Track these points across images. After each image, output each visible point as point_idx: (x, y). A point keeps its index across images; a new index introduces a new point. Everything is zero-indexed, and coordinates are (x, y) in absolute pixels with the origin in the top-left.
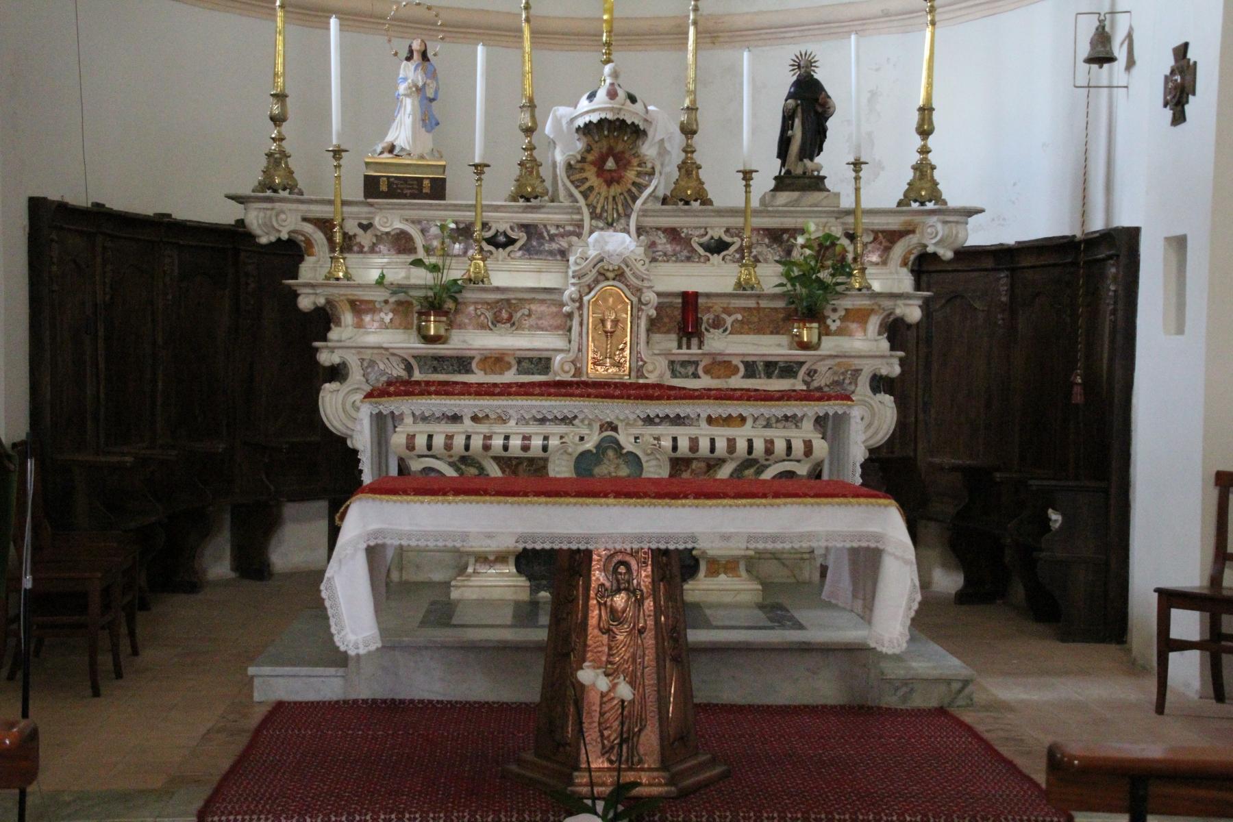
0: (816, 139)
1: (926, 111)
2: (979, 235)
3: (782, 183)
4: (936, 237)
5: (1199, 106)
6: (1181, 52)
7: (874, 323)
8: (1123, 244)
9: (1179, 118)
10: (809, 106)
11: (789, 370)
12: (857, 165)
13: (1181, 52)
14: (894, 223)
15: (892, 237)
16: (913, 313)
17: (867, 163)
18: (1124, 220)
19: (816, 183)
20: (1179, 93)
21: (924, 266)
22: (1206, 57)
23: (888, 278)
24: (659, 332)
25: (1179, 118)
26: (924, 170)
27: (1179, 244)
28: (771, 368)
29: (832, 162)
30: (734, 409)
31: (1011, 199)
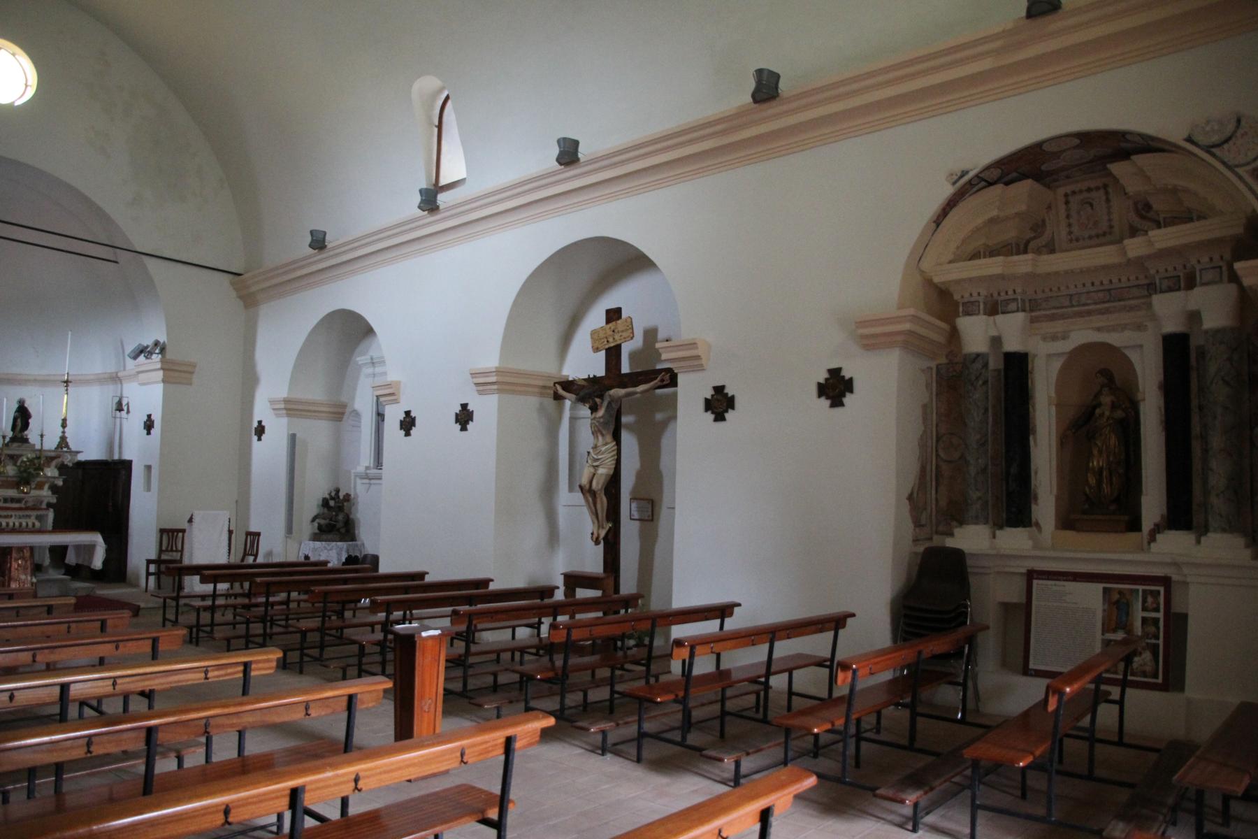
0: (26, 425)
1: (64, 421)
2: (81, 457)
3: (13, 440)
4: (68, 460)
5: (156, 430)
6: (149, 416)
7: (46, 486)
8: (127, 465)
9: (149, 433)
10: (23, 415)
11: (19, 501)
12: (42, 436)
13: (149, 416)
14: (53, 454)
15: (52, 458)
16: (60, 483)
17: (45, 434)
18: (126, 457)
19: (26, 441)
20: (149, 425)
21: (62, 468)
22: (157, 419)
23: (51, 472)
24: (781, 639)
25: (149, 433)
26: (63, 438)
27: (149, 468)
28: (13, 500)
29: (32, 435)
30: (9, 513)
31: (90, 450)
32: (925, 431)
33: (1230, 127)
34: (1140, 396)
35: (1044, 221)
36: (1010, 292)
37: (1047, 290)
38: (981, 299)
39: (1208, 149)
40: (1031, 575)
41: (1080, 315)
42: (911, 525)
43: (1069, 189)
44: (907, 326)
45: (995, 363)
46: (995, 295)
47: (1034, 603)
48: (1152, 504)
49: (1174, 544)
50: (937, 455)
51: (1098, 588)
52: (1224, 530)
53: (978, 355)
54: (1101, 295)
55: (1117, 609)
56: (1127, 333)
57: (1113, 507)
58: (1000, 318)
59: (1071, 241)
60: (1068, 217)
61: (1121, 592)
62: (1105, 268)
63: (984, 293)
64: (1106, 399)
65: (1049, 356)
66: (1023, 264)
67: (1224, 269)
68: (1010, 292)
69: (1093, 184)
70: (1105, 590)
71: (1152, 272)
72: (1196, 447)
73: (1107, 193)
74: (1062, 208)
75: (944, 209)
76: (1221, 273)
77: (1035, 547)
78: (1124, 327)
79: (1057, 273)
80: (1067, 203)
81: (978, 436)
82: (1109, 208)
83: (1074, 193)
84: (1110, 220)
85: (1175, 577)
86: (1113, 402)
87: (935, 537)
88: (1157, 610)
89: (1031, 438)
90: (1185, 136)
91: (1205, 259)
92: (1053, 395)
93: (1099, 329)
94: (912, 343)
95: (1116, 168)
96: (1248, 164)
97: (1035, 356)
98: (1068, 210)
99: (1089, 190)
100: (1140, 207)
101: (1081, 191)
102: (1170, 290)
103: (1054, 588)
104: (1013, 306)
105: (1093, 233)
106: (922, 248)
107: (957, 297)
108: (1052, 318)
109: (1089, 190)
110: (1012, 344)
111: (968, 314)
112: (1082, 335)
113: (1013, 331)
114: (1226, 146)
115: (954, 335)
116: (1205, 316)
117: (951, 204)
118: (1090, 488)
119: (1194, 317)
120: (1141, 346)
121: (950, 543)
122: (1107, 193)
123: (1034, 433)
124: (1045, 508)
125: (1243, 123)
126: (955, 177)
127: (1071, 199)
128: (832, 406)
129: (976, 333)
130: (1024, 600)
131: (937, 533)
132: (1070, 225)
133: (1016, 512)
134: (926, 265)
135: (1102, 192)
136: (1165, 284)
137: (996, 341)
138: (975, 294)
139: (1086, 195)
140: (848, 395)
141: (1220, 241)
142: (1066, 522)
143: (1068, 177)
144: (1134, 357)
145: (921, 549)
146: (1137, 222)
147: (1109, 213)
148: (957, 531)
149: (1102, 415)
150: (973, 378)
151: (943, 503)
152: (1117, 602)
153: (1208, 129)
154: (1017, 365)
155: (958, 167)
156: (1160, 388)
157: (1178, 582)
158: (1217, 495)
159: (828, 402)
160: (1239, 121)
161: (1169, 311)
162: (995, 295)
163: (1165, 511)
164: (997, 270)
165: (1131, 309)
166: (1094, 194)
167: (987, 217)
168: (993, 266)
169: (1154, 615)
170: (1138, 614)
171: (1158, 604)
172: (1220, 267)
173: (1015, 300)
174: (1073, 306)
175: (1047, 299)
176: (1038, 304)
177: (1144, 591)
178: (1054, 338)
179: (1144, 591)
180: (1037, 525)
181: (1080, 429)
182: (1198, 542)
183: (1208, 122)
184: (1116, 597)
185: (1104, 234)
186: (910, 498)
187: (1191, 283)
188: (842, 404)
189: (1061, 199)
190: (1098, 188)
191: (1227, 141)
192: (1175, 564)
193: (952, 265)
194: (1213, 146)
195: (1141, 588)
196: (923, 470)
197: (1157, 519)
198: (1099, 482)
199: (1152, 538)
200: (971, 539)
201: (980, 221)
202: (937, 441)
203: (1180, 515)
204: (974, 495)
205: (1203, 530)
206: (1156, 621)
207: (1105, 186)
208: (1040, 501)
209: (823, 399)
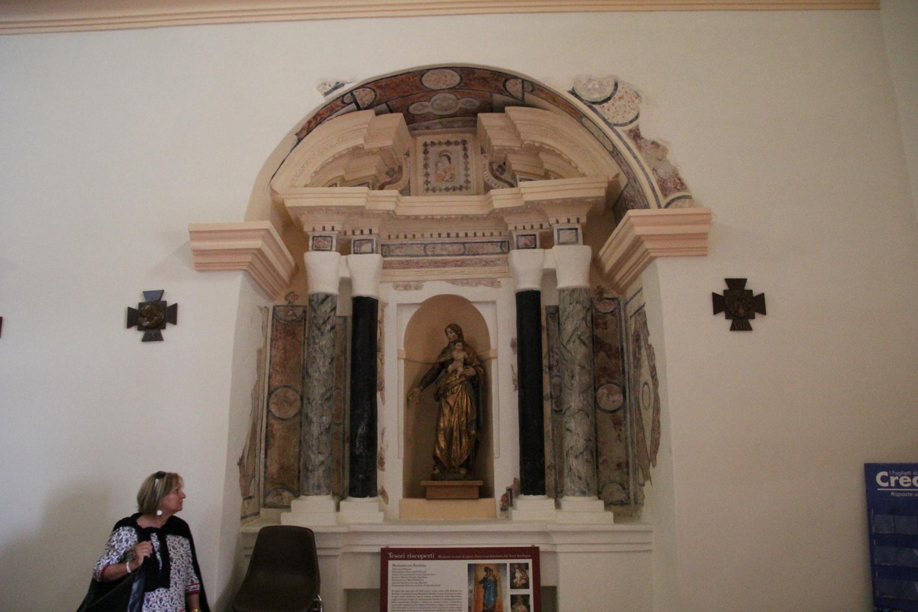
32: (258, 382)
33: (609, 90)
34: (492, 354)
35: (400, 168)
36: (366, 232)
37: (402, 236)
38: (334, 235)
39: (591, 104)
40: (386, 555)
41: (436, 264)
42: (240, 499)
43: (429, 139)
44: (258, 243)
45: (345, 309)
46: (349, 233)
47: (391, 589)
48: (505, 464)
49: (533, 510)
50: (268, 411)
51: (462, 565)
52: (583, 493)
53: (327, 296)
54: (456, 247)
55: (485, 584)
56: (481, 289)
57: (463, 472)
58: (352, 257)
59: (427, 190)
60: (426, 166)
61: (487, 569)
62: (465, 218)
63: (338, 227)
64: (459, 355)
65: (400, 306)
66: (387, 200)
67: (580, 231)
68: (366, 232)
69: (452, 138)
70: (470, 567)
71: (511, 228)
72: (548, 407)
73: (465, 149)
74: (421, 156)
75: (309, 122)
76: (577, 234)
77: (386, 520)
78: (477, 282)
79: (417, 218)
80: (426, 152)
81: (323, 390)
82: (466, 163)
83: (433, 143)
84: (467, 175)
85: (542, 548)
86: (465, 360)
87: (263, 511)
88: (526, 586)
89: (378, 394)
90: (570, 89)
91: (563, 220)
92: (402, 348)
93: (453, 282)
94: (257, 268)
95: (485, 119)
96: (626, 124)
97: (385, 305)
98: (426, 159)
99: (448, 143)
100: (495, 167)
101: (440, 143)
102: (527, 247)
103: (414, 569)
104: (367, 247)
105: (450, 185)
106: (278, 163)
107: (307, 228)
108: (406, 265)
109: (448, 143)
110: (363, 289)
111: (318, 249)
112: (435, 285)
113: (366, 274)
114: (605, 104)
115: (299, 271)
116: (559, 276)
117: (317, 119)
118: (441, 450)
119: (550, 276)
120: (494, 302)
121: (288, 519)
122: (465, 149)
123: (382, 389)
124: (392, 473)
125: (620, 87)
126: (329, 88)
127: (431, 149)
128: (146, 339)
129: (326, 271)
130: (377, 585)
131: (265, 505)
132: (427, 175)
133: (361, 480)
134: (278, 184)
135: (459, 148)
136: (522, 241)
137: (346, 283)
138: (328, 228)
139: (444, 147)
140: (169, 326)
141: (580, 202)
142: (414, 490)
143: (427, 128)
144: (486, 313)
145: (255, 527)
146: (492, 181)
147: (466, 169)
148: (294, 503)
149: (455, 371)
150: (321, 322)
151: (274, 468)
152: (485, 580)
153: (590, 86)
154: (366, 311)
155: (333, 78)
156: (513, 345)
157: (546, 552)
158: (576, 457)
159: (141, 335)
160: (616, 85)
161: (527, 269)
162: (349, 233)
163: (517, 475)
164: (360, 202)
165: (487, 263)
166: (451, 148)
167: (351, 144)
168: (356, 197)
169: (395, 588)
170: (507, 592)
171: (527, 580)
172: (576, 229)
173: (370, 241)
174: (427, 255)
175: (402, 245)
176: (396, 246)
177: (512, 565)
178: (407, 287)
179: (512, 565)
180: (384, 493)
181: (429, 383)
182: (558, 506)
183: (590, 80)
184: (482, 574)
185: (461, 188)
186: (241, 463)
187: (546, 241)
188: (159, 338)
189: (421, 149)
190: (456, 143)
191: (607, 100)
192: (545, 534)
193: (308, 189)
194: (594, 103)
195: (508, 562)
196: (254, 426)
197: (510, 484)
198: (449, 444)
199: (508, 502)
200: (312, 512)
201: (342, 147)
202: (270, 394)
203: (534, 479)
204: (317, 459)
205: (557, 494)
206: (525, 598)
207: (464, 142)
208: (386, 466)
209: (134, 330)
